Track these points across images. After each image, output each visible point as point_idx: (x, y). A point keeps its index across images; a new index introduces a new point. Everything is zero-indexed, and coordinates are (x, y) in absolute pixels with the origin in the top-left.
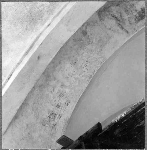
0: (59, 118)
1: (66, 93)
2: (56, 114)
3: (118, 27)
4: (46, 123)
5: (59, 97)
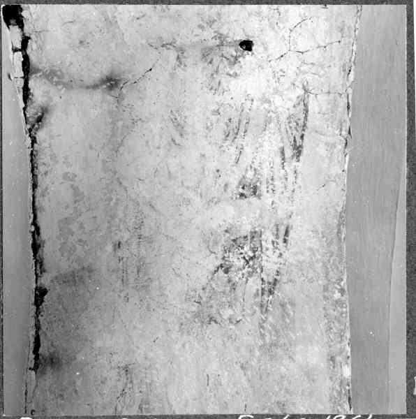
0: (280, 241)
1: (255, 103)
2: (255, 235)
3: (44, 242)
4: (221, 305)
5: (228, 143)
